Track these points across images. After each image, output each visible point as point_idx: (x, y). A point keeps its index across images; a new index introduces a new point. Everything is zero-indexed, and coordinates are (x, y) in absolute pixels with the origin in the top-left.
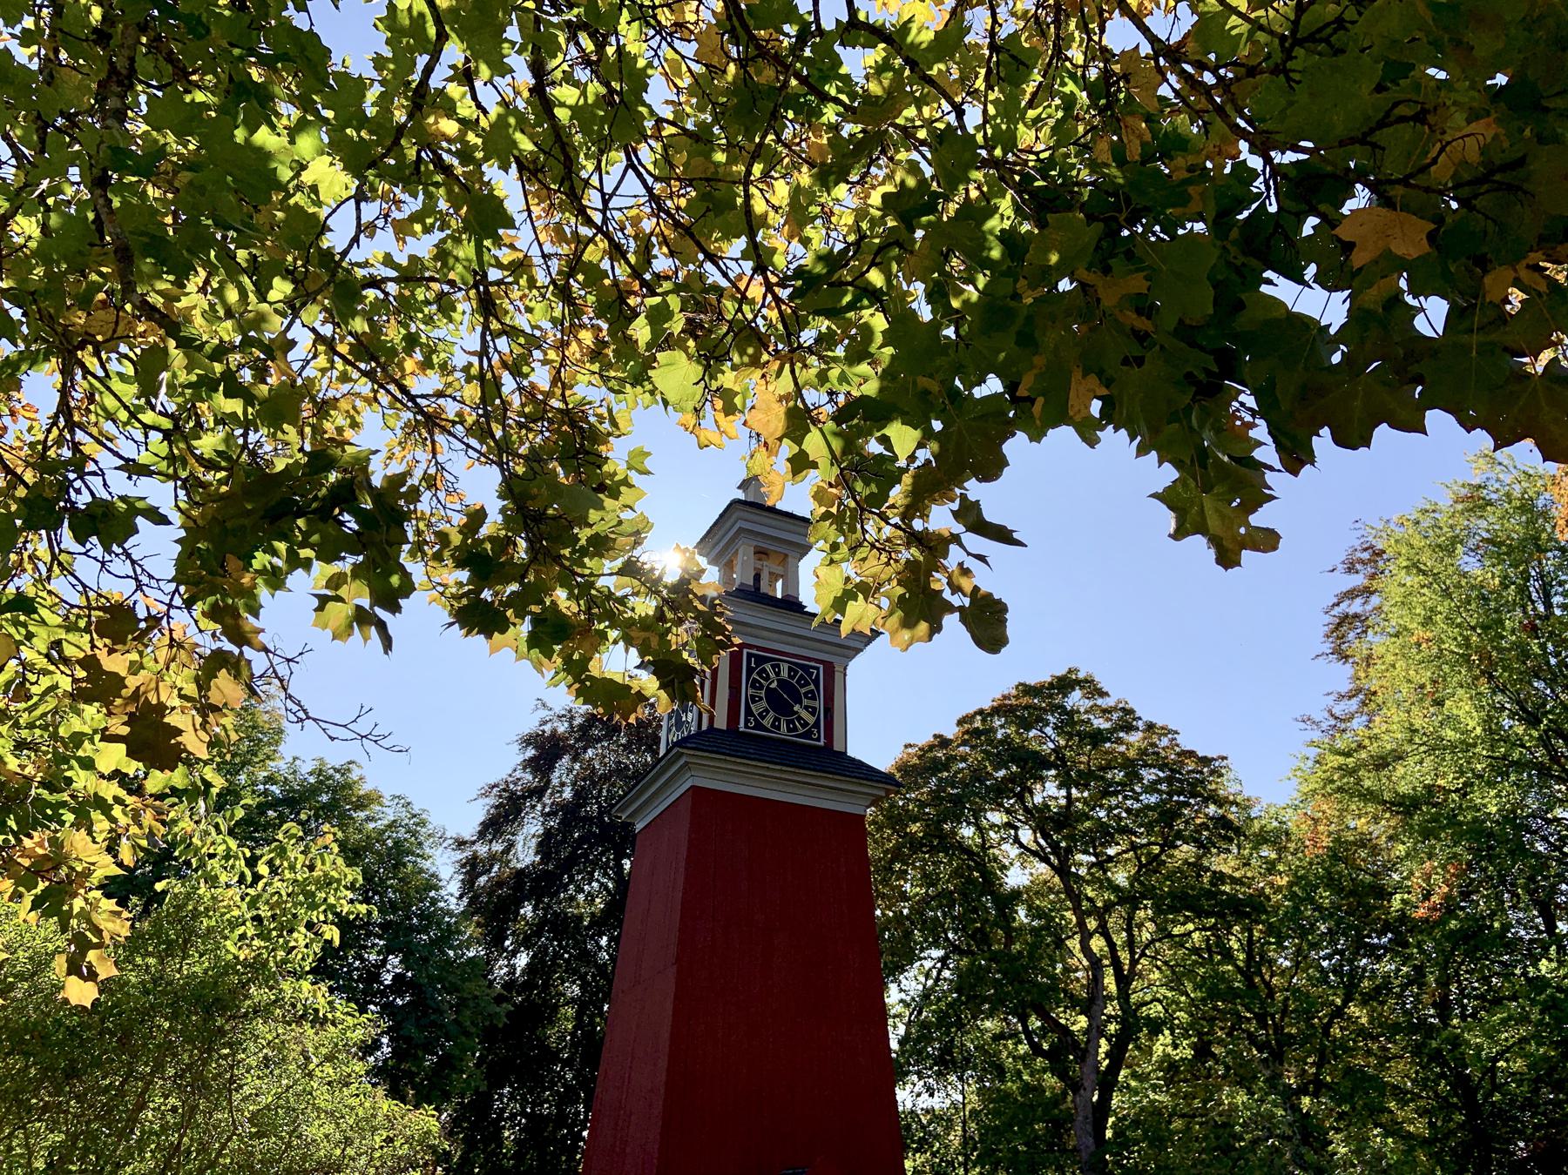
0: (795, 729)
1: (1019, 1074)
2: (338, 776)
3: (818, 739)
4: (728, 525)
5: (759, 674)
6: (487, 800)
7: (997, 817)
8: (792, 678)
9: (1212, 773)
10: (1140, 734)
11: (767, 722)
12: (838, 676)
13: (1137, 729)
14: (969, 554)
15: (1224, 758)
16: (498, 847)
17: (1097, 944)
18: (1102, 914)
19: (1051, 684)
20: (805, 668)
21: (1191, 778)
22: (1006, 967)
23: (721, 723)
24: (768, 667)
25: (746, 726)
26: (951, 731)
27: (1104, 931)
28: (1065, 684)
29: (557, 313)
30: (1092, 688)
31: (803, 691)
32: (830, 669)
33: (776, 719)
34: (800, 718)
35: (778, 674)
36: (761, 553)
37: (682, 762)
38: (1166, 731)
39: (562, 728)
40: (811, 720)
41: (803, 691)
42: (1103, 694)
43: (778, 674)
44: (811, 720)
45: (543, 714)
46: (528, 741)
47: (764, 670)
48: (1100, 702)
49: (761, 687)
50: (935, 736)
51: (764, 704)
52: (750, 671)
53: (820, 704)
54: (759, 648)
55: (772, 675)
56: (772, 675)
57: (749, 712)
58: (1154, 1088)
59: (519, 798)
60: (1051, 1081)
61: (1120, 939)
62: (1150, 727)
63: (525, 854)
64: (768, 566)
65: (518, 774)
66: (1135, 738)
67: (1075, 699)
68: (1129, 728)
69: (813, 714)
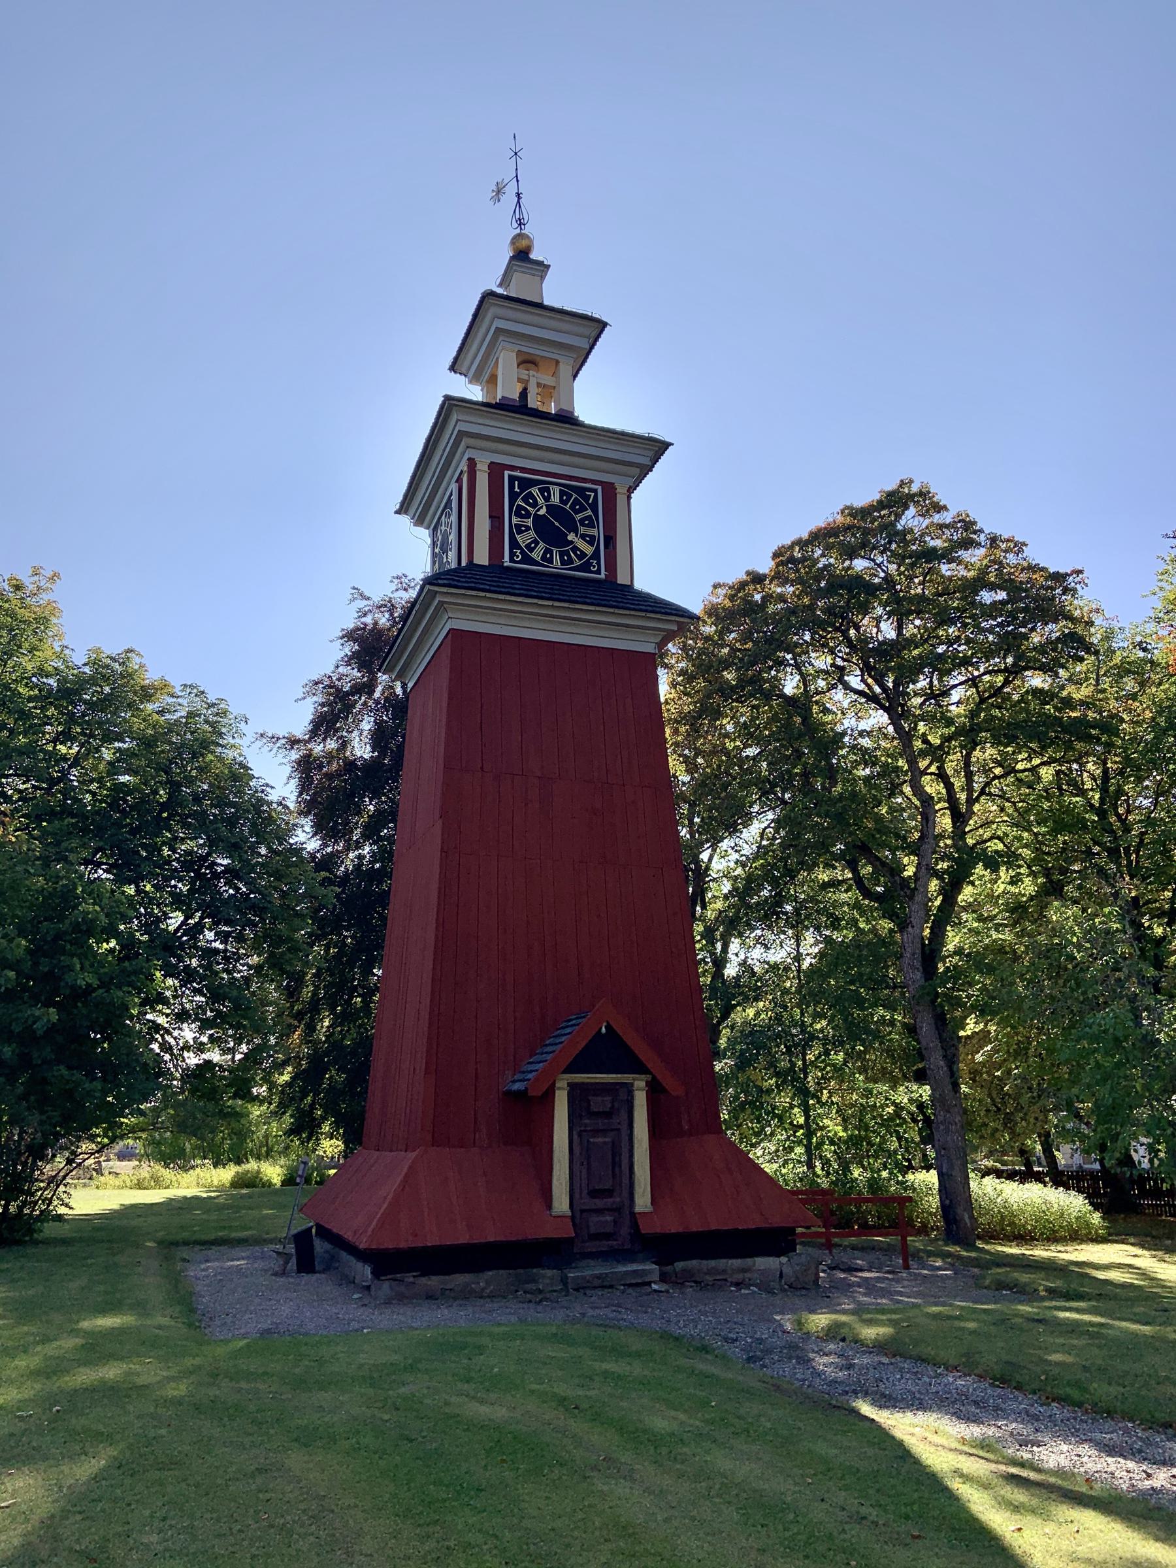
0: (571, 561)
1: (855, 922)
2: (116, 666)
3: (598, 572)
4: (483, 330)
5: (525, 500)
6: (315, 698)
7: (822, 661)
9: (1066, 591)
10: (983, 551)
11: (537, 555)
12: (621, 500)
13: (979, 545)
15: (1080, 572)
16: (332, 745)
17: (932, 787)
18: (937, 753)
19: (880, 502)
20: (581, 491)
21: (1038, 598)
22: (832, 814)
23: (482, 557)
24: (535, 491)
25: (512, 560)
26: (765, 566)
27: (942, 776)
28: (896, 500)
30: (927, 503)
31: (578, 517)
32: (610, 490)
33: (547, 551)
34: (575, 549)
35: (547, 499)
36: (527, 361)
37: (436, 602)
38: (1019, 547)
39: (384, 620)
40: (589, 550)
41: (578, 517)
42: (939, 508)
43: (547, 499)
44: (589, 550)
45: (361, 604)
46: (350, 636)
47: (530, 495)
48: (937, 518)
49: (528, 515)
50: (748, 573)
51: (532, 534)
52: (513, 497)
53: (600, 532)
54: (523, 470)
55: (540, 501)
56: (540, 501)
57: (514, 544)
58: (997, 928)
59: (347, 694)
60: (886, 925)
61: (958, 783)
62: (994, 540)
63: (361, 749)
64: (535, 378)
65: (341, 670)
66: (975, 556)
67: (910, 519)
68: (968, 544)
69: (591, 543)
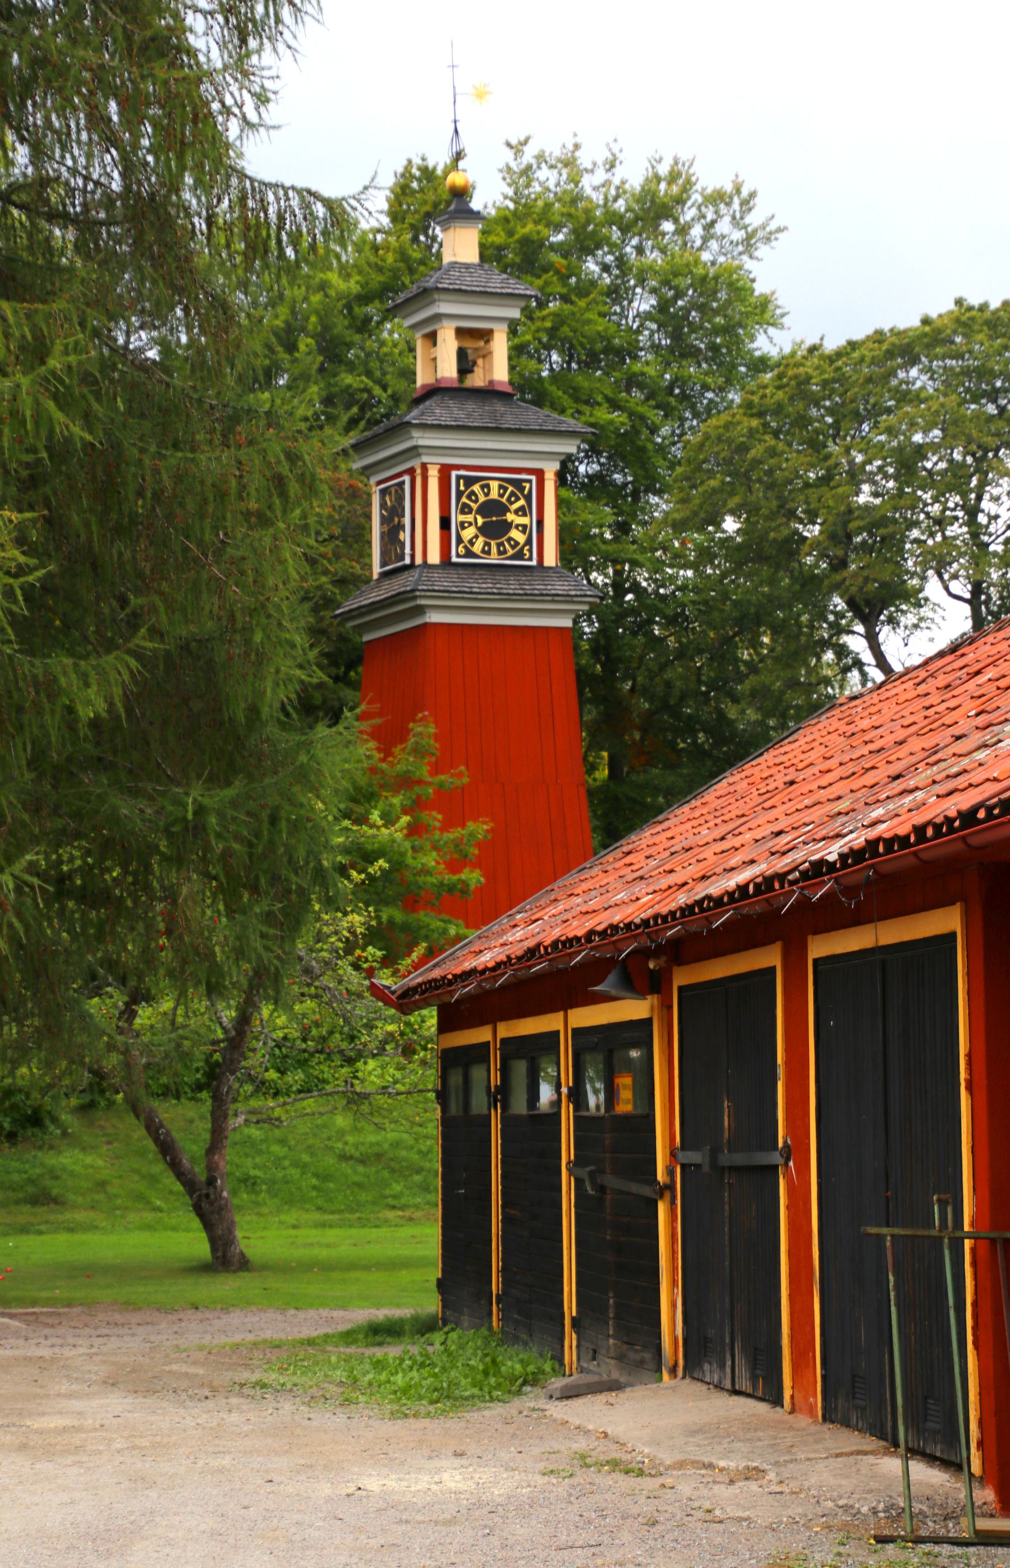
3: (530, 559)
5: (469, 497)
8: (502, 496)
11: (478, 547)
14: (988, 780)
20: (518, 484)
25: (458, 556)
29: (544, 174)
33: (487, 544)
47: (473, 493)
52: (459, 494)
57: (460, 540)
